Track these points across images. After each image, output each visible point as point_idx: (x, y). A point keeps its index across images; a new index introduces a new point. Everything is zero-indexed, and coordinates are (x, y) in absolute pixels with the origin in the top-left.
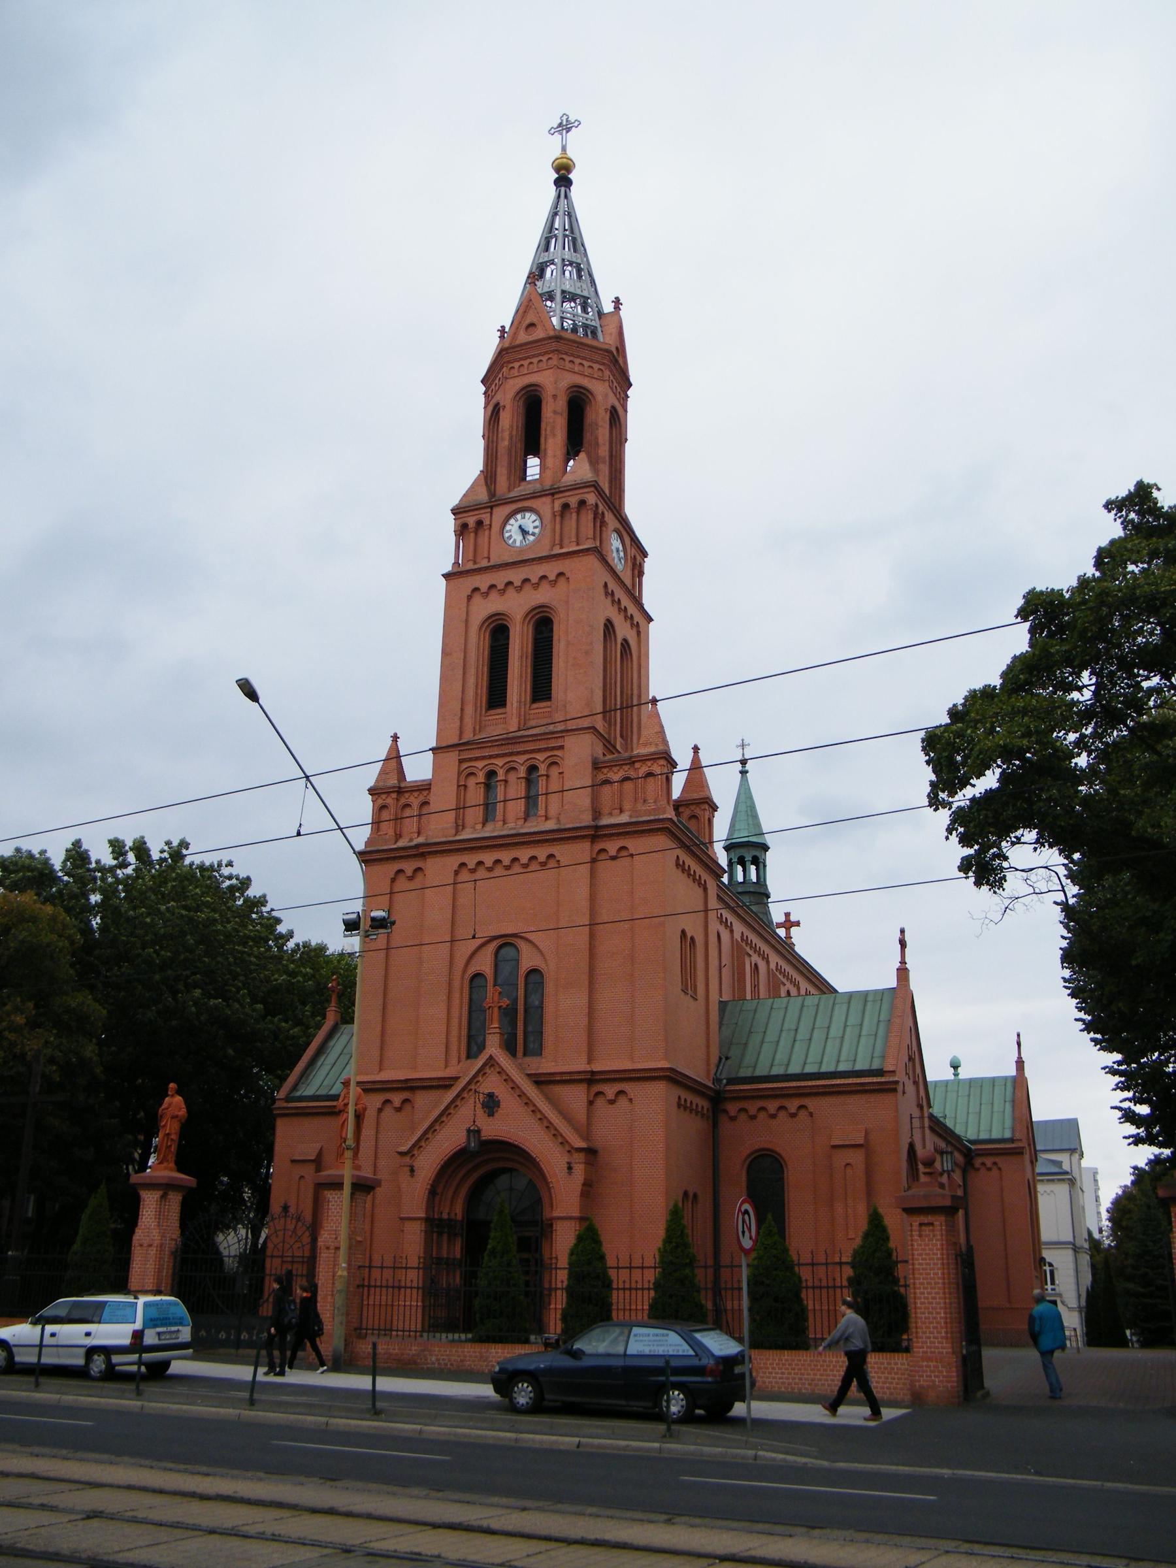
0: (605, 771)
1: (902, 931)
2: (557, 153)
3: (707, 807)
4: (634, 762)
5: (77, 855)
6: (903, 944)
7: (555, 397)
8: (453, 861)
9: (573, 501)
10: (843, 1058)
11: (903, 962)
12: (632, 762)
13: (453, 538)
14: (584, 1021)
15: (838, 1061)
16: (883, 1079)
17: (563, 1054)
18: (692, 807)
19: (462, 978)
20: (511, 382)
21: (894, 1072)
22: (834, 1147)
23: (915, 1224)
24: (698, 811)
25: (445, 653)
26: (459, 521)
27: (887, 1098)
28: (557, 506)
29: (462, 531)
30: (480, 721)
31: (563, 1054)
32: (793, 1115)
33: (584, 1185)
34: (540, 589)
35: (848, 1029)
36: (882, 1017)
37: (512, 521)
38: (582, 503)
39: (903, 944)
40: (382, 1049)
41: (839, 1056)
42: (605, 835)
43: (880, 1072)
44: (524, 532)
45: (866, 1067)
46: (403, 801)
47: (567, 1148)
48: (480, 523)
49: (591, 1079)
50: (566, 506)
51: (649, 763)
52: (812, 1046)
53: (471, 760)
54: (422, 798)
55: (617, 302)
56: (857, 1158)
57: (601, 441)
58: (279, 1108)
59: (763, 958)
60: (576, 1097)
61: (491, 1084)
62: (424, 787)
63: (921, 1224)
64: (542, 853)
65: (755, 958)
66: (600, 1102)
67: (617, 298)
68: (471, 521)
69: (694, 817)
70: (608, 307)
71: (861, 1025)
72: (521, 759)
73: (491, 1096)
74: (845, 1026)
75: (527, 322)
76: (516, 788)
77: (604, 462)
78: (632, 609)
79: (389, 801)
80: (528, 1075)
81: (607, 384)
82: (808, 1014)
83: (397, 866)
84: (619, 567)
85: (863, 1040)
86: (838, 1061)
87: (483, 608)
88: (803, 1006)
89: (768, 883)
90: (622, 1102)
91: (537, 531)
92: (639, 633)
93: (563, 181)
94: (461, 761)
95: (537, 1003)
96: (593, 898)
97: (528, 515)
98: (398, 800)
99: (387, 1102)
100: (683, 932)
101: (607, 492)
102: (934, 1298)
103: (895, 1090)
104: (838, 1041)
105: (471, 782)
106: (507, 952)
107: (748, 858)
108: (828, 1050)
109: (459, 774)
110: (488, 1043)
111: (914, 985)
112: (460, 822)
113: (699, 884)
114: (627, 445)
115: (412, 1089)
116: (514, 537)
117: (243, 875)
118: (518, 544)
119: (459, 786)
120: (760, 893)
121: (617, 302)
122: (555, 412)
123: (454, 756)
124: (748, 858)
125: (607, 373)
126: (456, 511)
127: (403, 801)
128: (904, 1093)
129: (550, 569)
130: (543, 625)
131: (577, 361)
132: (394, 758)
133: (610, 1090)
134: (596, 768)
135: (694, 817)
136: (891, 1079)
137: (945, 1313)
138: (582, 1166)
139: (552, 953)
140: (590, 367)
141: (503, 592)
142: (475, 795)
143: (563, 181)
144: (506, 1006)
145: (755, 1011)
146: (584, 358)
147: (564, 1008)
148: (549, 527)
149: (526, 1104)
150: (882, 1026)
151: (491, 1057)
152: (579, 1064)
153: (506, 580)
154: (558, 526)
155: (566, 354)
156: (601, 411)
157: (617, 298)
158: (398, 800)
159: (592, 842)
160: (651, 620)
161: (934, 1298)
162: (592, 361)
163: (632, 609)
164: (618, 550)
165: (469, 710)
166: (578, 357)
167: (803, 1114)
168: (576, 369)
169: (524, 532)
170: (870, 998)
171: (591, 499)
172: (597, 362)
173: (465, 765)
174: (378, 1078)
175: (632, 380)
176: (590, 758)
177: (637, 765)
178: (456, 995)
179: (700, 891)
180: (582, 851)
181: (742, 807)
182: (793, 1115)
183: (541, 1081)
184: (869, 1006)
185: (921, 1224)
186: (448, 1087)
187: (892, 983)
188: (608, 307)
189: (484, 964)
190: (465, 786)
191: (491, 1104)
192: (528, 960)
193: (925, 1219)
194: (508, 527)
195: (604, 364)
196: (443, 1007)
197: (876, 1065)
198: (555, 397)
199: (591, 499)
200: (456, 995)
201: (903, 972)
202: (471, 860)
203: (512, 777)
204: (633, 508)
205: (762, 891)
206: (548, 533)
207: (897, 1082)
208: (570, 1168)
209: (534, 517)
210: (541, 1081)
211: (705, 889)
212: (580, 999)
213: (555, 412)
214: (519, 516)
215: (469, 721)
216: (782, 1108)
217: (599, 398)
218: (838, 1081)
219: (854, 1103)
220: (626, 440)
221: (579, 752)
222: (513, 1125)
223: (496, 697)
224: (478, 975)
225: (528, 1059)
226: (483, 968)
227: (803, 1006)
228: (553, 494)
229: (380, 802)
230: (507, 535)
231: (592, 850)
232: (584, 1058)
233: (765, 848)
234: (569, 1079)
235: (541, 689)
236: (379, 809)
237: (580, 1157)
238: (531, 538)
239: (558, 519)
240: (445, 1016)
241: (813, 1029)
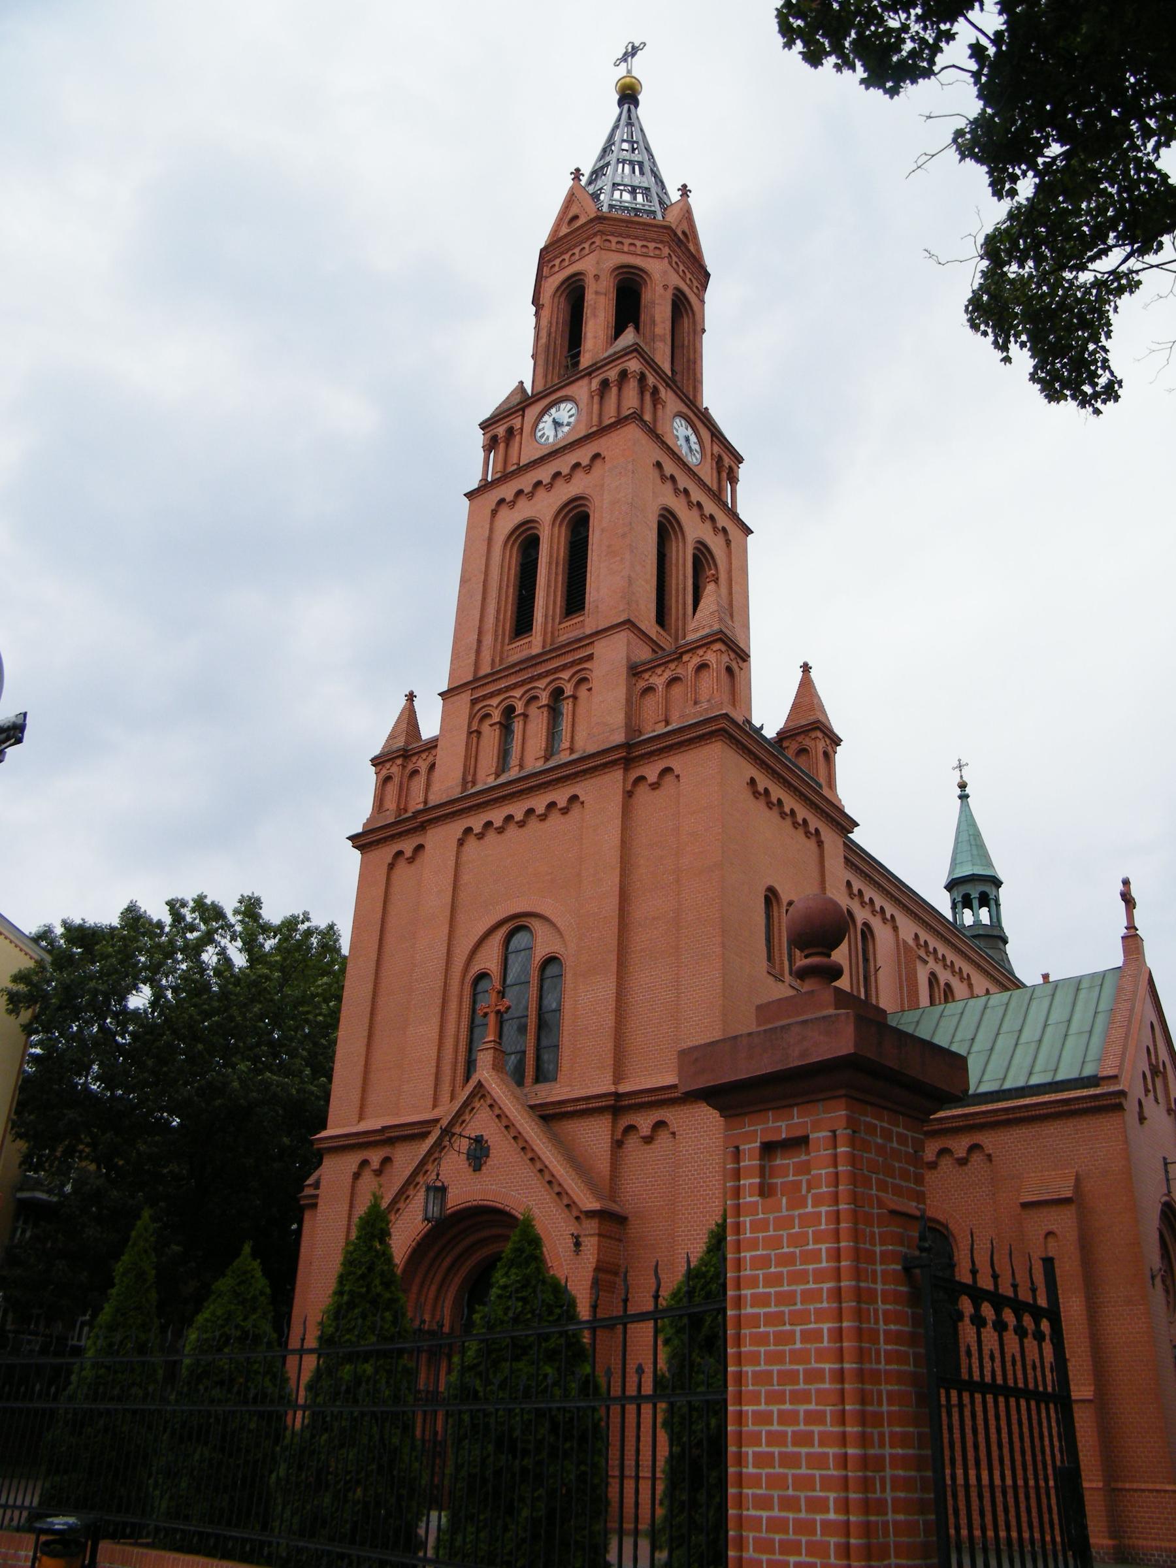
0: (646, 676)
1: (1126, 882)
2: (958, 780)
3: (820, 735)
4: (682, 654)
5: (133, 918)
6: (1129, 901)
7: (597, 277)
8: (455, 829)
9: (612, 374)
10: (1037, 1069)
11: (1131, 927)
12: (678, 656)
13: (481, 454)
14: (610, 1020)
15: (1031, 1074)
16: (1098, 1091)
17: (583, 1075)
18: (800, 739)
19: (462, 983)
20: (550, 280)
21: (1115, 1077)
22: (1025, 1205)
23: (751, 1147)
24: (807, 742)
25: (463, 581)
26: (489, 435)
27: (1106, 1124)
28: (595, 384)
29: (491, 445)
30: (502, 652)
31: (583, 1075)
32: (962, 1162)
33: (597, 1269)
34: (573, 481)
35: (1049, 1030)
36: (1103, 1006)
37: (546, 418)
38: (624, 374)
39: (1129, 901)
40: (364, 1090)
41: (1033, 1067)
42: (642, 756)
43: (1094, 1081)
44: (557, 424)
45: (1074, 1074)
46: (410, 767)
47: (575, 1213)
48: (510, 432)
49: (617, 1106)
50: (605, 384)
51: (701, 652)
52: (994, 1057)
53: (485, 697)
54: (667, 675)
55: (685, 191)
56: (1063, 1222)
57: (658, 318)
58: (306, 1197)
59: (962, 979)
60: (594, 1136)
61: (481, 1124)
62: (433, 744)
63: (769, 1149)
64: (560, 796)
65: (932, 965)
66: (632, 1142)
67: (685, 186)
68: (501, 431)
69: (803, 751)
70: (675, 196)
71: (1069, 1021)
72: (541, 684)
73: (478, 1140)
74: (1045, 1026)
75: (570, 215)
76: (538, 722)
77: (663, 340)
78: (722, 520)
79: (395, 770)
80: (532, 1107)
81: (666, 261)
82: (992, 1018)
83: (395, 847)
84: (693, 460)
85: (1070, 1041)
86: (1031, 1074)
87: (508, 520)
88: (985, 1008)
89: (1004, 925)
90: (663, 1137)
91: (572, 420)
92: (728, 542)
93: (964, 797)
94: (474, 702)
95: (554, 1006)
96: (625, 844)
97: (563, 406)
98: (404, 767)
99: (365, 1163)
100: (771, 897)
101: (669, 374)
102: (803, 1439)
103: (1119, 1108)
104: (1033, 1046)
105: (485, 727)
106: (520, 940)
107: (975, 895)
108: (1015, 1062)
109: (472, 717)
110: (479, 1064)
111: (1153, 958)
112: (470, 778)
113: (807, 834)
114: (706, 337)
115: (391, 1142)
116: (547, 433)
117: (323, 925)
118: (551, 440)
119: (470, 733)
120: (995, 937)
121: (685, 191)
122: (597, 293)
123: (465, 698)
124: (975, 895)
125: (666, 251)
126: (485, 426)
127: (410, 767)
128: (1142, 1119)
129: (583, 455)
130: (577, 520)
131: (627, 241)
132: (409, 718)
133: (644, 1122)
134: (634, 675)
135: (803, 751)
136: (1112, 1089)
137: (844, 1506)
138: (594, 1240)
139: (574, 926)
140: (643, 246)
141: (531, 495)
142: (491, 737)
143: (964, 797)
144: (511, 1014)
145: (918, 1022)
146: (636, 238)
147: (585, 1004)
148: (584, 413)
149: (523, 1149)
150: (1101, 1018)
151: (480, 1085)
152: (603, 1084)
153: (535, 480)
154: (596, 407)
155: (612, 234)
156: (659, 289)
157: (685, 186)
158: (404, 767)
159: (626, 770)
160: (748, 531)
161: (803, 1439)
162: (646, 239)
163: (722, 520)
164: (687, 439)
165: (488, 640)
166: (628, 237)
167: (976, 1158)
168: (626, 249)
169: (557, 424)
170: (1084, 985)
171: (634, 365)
172: (653, 241)
173: (478, 707)
174: (354, 1130)
175: (709, 269)
176: (624, 662)
177: (685, 658)
178: (453, 1005)
179: (811, 844)
180: (614, 781)
181: (964, 837)
182: (962, 1162)
183: (550, 1116)
184: (1082, 995)
185: (769, 1149)
186: (424, 1135)
187: (1116, 958)
188: (675, 196)
189: (489, 960)
190: (479, 733)
191: (479, 1154)
192: (544, 944)
193: (781, 1126)
194: (541, 426)
195: (661, 242)
196: (435, 1021)
197: (1088, 1071)
198: (597, 277)
199: (634, 365)
200: (453, 1005)
201: (1132, 941)
202: (476, 822)
203: (533, 710)
204: (712, 398)
205: (995, 933)
206: (584, 418)
207: (1122, 1094)
208: (577, 1244)
209: (569, 405)
210: (550, 1116)
211: (820, 844)
212: (605, 988)
213: (597, 293)
214: (553, 411)
215: (486, 656)
216: (944, 1152)
217: (656, 276)
218: (1027, 1101)
219: (1057, 1134)
220: (704, 331)
221: (611, 658)
222: (507, 1185)
223: (522, 624)
224: (483, 976)
225: (538, 1087)
226: (488, 965)
227: (985, 1008)
228: (590, 374)
229: (384, 772)
230: (539, 434)
231: (624, 780)
232: (609, 1077)
233: (997, 883)
234: (585, 1109)
235: (574, 599)
236: (384, 782)
237: (591, 1226)
238: (566, 429)
239: (596, 399)
240: (436, 1036)
241: (998, 1034)
